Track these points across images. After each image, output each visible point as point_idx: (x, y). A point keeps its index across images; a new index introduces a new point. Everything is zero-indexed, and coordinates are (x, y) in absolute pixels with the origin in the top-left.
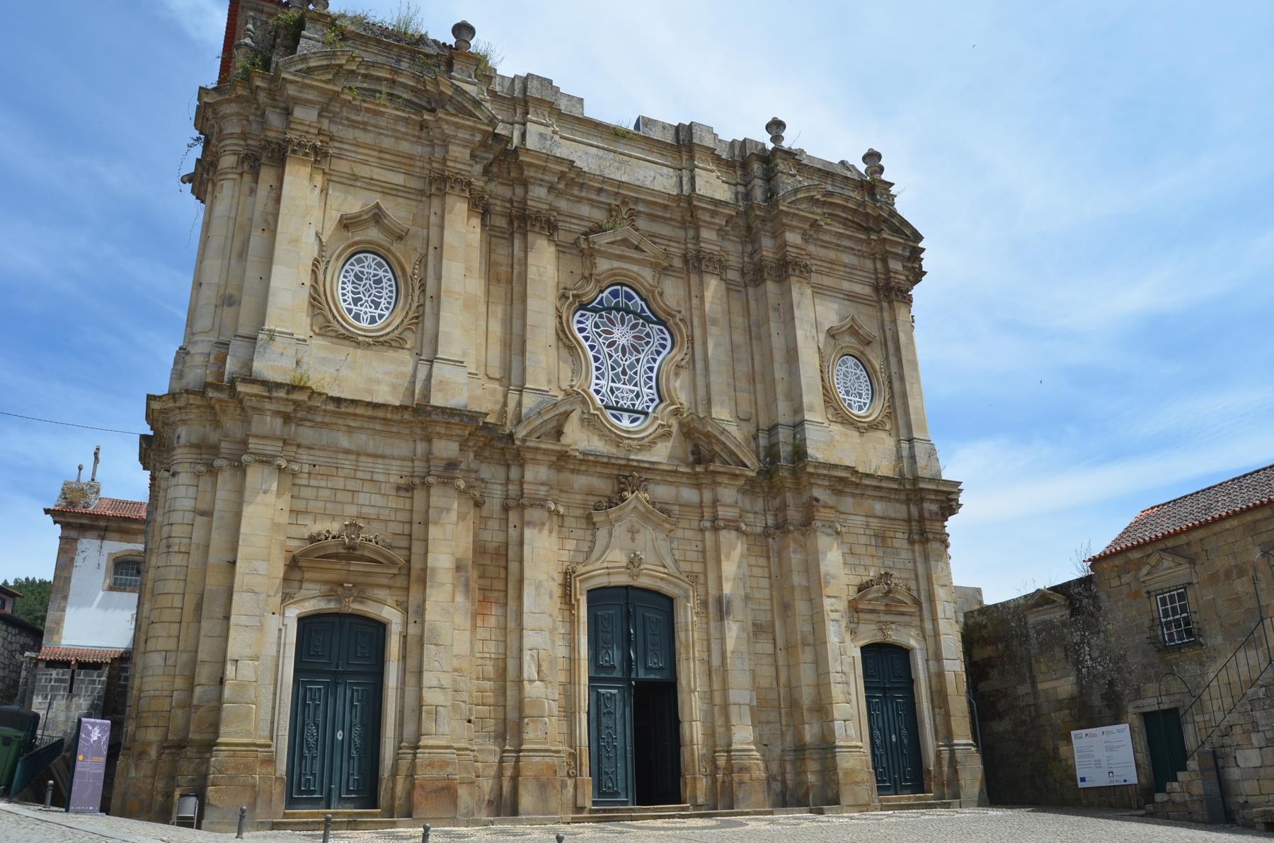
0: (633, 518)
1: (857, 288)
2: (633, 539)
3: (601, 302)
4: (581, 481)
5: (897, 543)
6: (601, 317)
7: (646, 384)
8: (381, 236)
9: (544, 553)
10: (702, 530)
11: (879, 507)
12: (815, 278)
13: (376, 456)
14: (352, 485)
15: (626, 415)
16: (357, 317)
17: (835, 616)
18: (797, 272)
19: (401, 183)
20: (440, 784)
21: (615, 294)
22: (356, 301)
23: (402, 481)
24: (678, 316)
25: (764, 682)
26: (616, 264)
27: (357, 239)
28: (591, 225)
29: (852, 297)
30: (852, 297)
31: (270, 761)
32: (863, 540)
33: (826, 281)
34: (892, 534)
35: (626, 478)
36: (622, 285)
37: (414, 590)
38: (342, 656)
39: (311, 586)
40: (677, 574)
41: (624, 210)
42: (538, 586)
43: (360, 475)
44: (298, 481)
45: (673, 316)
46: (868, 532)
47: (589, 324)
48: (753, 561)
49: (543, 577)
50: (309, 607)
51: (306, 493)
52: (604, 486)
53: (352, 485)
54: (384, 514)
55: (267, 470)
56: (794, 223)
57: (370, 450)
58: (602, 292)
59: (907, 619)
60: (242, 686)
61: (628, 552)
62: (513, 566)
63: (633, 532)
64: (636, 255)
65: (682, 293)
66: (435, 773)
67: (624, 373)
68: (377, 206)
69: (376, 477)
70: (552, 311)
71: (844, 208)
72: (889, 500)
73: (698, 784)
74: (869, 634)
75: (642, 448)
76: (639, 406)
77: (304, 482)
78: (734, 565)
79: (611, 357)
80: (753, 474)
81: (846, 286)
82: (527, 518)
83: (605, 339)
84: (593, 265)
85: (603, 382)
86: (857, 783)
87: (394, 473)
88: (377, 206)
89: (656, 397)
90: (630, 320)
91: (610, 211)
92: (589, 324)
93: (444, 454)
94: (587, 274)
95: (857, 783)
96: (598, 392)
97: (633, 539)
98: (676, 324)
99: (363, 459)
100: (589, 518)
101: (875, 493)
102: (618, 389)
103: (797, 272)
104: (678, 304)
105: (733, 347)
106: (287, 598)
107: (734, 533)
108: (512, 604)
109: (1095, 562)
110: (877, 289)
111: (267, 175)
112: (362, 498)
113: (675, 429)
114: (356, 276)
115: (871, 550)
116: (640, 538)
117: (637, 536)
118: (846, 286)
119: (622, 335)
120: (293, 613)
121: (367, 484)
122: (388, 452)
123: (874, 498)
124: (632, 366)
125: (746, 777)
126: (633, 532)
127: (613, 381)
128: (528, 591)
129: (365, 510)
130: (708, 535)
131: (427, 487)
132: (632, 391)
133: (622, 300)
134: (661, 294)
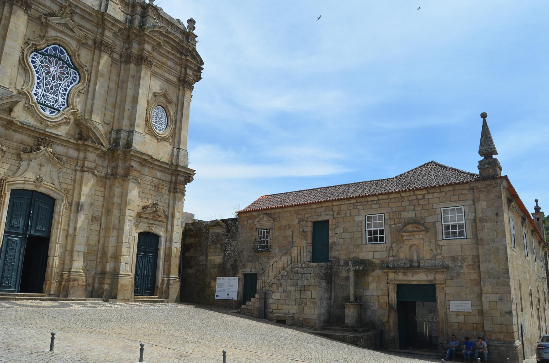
1: (171, 78)
2: (40, 169)
3: (47, 51)
4: (18, 136)
5: (163, 191)
6: (45, 58)
7: (62, 96)
11: (159, 174)
15: (48, 109)
17: (130, 218)
18: (146, 64)
21: (55, 49)
24: (85, 68)
26: (59, 35)
29: (168, 81)
32: (149, 187)
33: (158, 70)
34: (162, 187)
35: (42, 139)
36: (60, 45)
40: (60, 189)
41: (69, 9)
45: (83, 68)
46: (152, 184)
47: (38, 60)
48: (97, 188)
56: (150, 41)
58: (48, 46)
59: (161, 223)
63: (41, 165)
67: (52, 88)
70: (19, 48)
71: (174, 41)
72: (164, 172)
73: (52, 285)
74: (144, 228)
75: (53, 127)
76: (56, 106)
78: (88, 188)
79: (46, 79)
80: (106, 150)
81: (166, 75)
84: (47, 32)
85: (39, 90)
86: (125, 290)
89: (66, 103)
90: (60, 64)
92: (38, 60)
94: (42, 35)
95: (125, 290)
96: (36, 95)
97: (40, 169)
98: (83, 72)
101: (158, 168)
102: (47, 95)
103: (146, 64)
105: (109, 89)
110: (179, 80)
113: (72, 121)
115: (152, 192)
116: (44, 169)
118: (166, 75)
119: (54, 70)
123: (158, 170)
124: (56, 86)
126: (41, 165)
127: (45, 91)
132: (54, 98)
133: (58, 53)
134: (79, 55)
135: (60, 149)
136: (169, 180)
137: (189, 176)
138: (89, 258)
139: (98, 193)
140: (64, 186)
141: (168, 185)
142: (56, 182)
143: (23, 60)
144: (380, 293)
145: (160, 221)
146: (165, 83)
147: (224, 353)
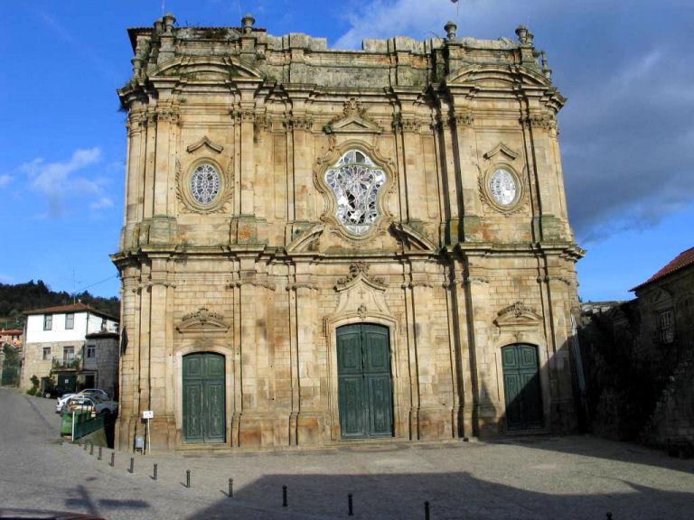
0: (361, 285)
1: (507, 123)
4: (330, 268)
8: (210, 153)
9: (309, 311)
10: (403, 288)
12: (476, 123)
13: (213, 272)
14: (204, 288)
16: (201, 200)
18: (462, 123)
19: (219, 120)
20: (252, 431)
22: (200, 191)
23: (228, 284)
25: (550, 356)
26: (350, 137)
27: (198, 157)
28: (332, 117)
29: (503, 130)
30: (503, 130)
31: (174, 423)
35: (356, 261)
37: (237, 338)
38: (204, 375)
39: (188, 340)
40: (388, 313)
41: (353, 103)
42: (306, 329)
43: (207, 283)
44: (176, 289)
46: (509, 278)
48: (437, 302)
49: (307, 323)
50: (186, 351)
51: (182, 295)
52: (344, 269)
53: (204, 288)
54: (220, 301)
55: (161, 287)
57: (211, 270)
59: (533, 328)
60: (158, 389)
61: (361, 303)
62: (293, 319)
63: (362, 293)
64: (361, 130)
65: (392, 147)
66: (248, 426)
68: (206, 138)
69: (215, 283)
70: (310, 173)
73: (233, 433)
74: (506, 337)
77: (180, 290)
81: (499, 123)
82: (298, 293)
83: (359, 170)
87: (222, 281)
88: (206, 138)
91: (344, 105)
93: (247, 268)
94: (331, 148)
99: (208, 274)
100: (335, 288)
103: (462, 123)
104: (390, 154)
105: (427, 174)
106: (175, 349)
107: (422, 288)
108: (293, 339)
109: (638, 290)
110: (521, 121)
111: (151, 131)
112: (210, 295)
114: (199, 178)
116: (366, 297)
117: (58, 415)
120: (179, 354)
121: (211, 287)
122: (220, 270)
125: (427, 423)
126: (362, 293)
128: (301, 332)
129: (210, 300)
130: (408, 290)
131: (239, 286)
134: (378, 150)
135: (378, 268)
136: (401, 271)
137: (86, 294)
138: (442, 388)
139: (440, 307)
140: (393, 309)
141: (536, 271)
142: (384, 307)
143: (318, 183)
144: (81, 379)
145: (530, 325)
146: (499, 134)
147: (188, 473)
